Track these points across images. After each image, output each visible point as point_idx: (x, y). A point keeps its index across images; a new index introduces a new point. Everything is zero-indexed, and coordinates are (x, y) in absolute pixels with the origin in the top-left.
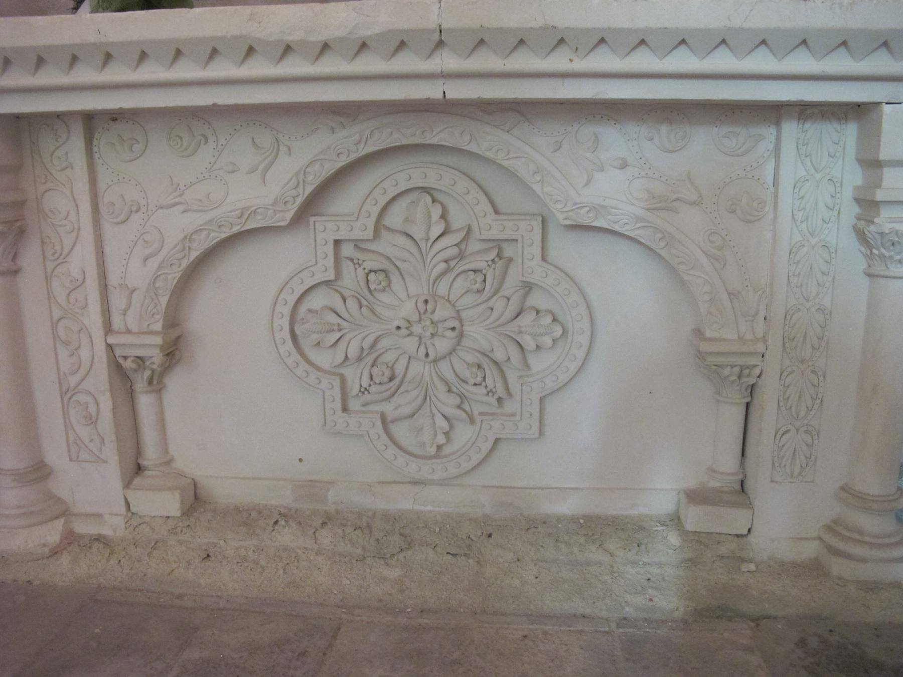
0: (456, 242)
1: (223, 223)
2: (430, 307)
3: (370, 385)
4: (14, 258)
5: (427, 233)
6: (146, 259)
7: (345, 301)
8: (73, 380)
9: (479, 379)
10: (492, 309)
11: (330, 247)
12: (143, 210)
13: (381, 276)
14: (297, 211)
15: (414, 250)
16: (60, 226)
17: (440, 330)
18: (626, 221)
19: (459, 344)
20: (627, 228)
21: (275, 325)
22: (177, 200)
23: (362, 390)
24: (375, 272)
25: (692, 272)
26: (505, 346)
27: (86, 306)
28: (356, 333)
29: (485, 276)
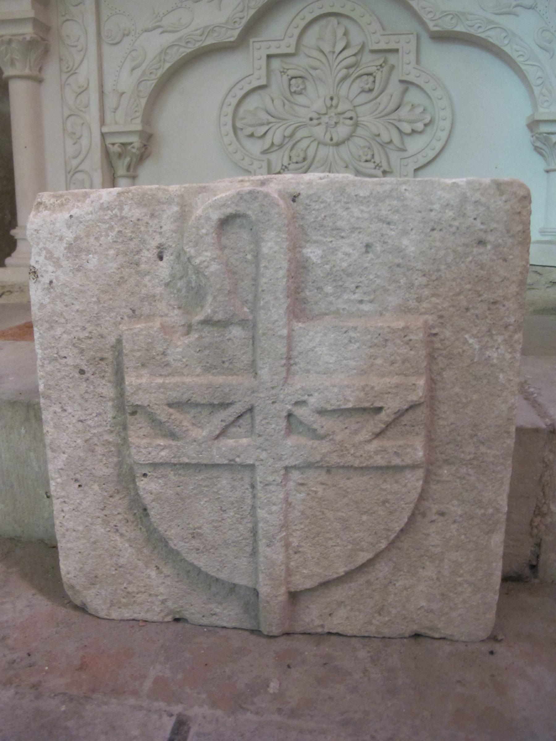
0: (354, 53)
1: (190, 40)
2: (334, 102)
3: (289, 164)
4: (40, 70)
5: (334, 47)
6: (133, 69)
7: (273, 101)
8: (75, 163)
9: (369, 157)
10: (380, 104)
11: (263, 62)
12: (133, 33)
13: (300, 81)
14: (242, 30)
15: (323, 59)
16: (73, 46)
17: (342, 120)
18: (479, 25)
19: (354, 131)
20: (480, 30)
21: (233, 90)
22: (157, 24)
23: (284, 167)
24: (296, 78)
25: (529, 63)
26: (388, 129)
27: (87, 106)
28: (280, 124)
29: (375, 77)
